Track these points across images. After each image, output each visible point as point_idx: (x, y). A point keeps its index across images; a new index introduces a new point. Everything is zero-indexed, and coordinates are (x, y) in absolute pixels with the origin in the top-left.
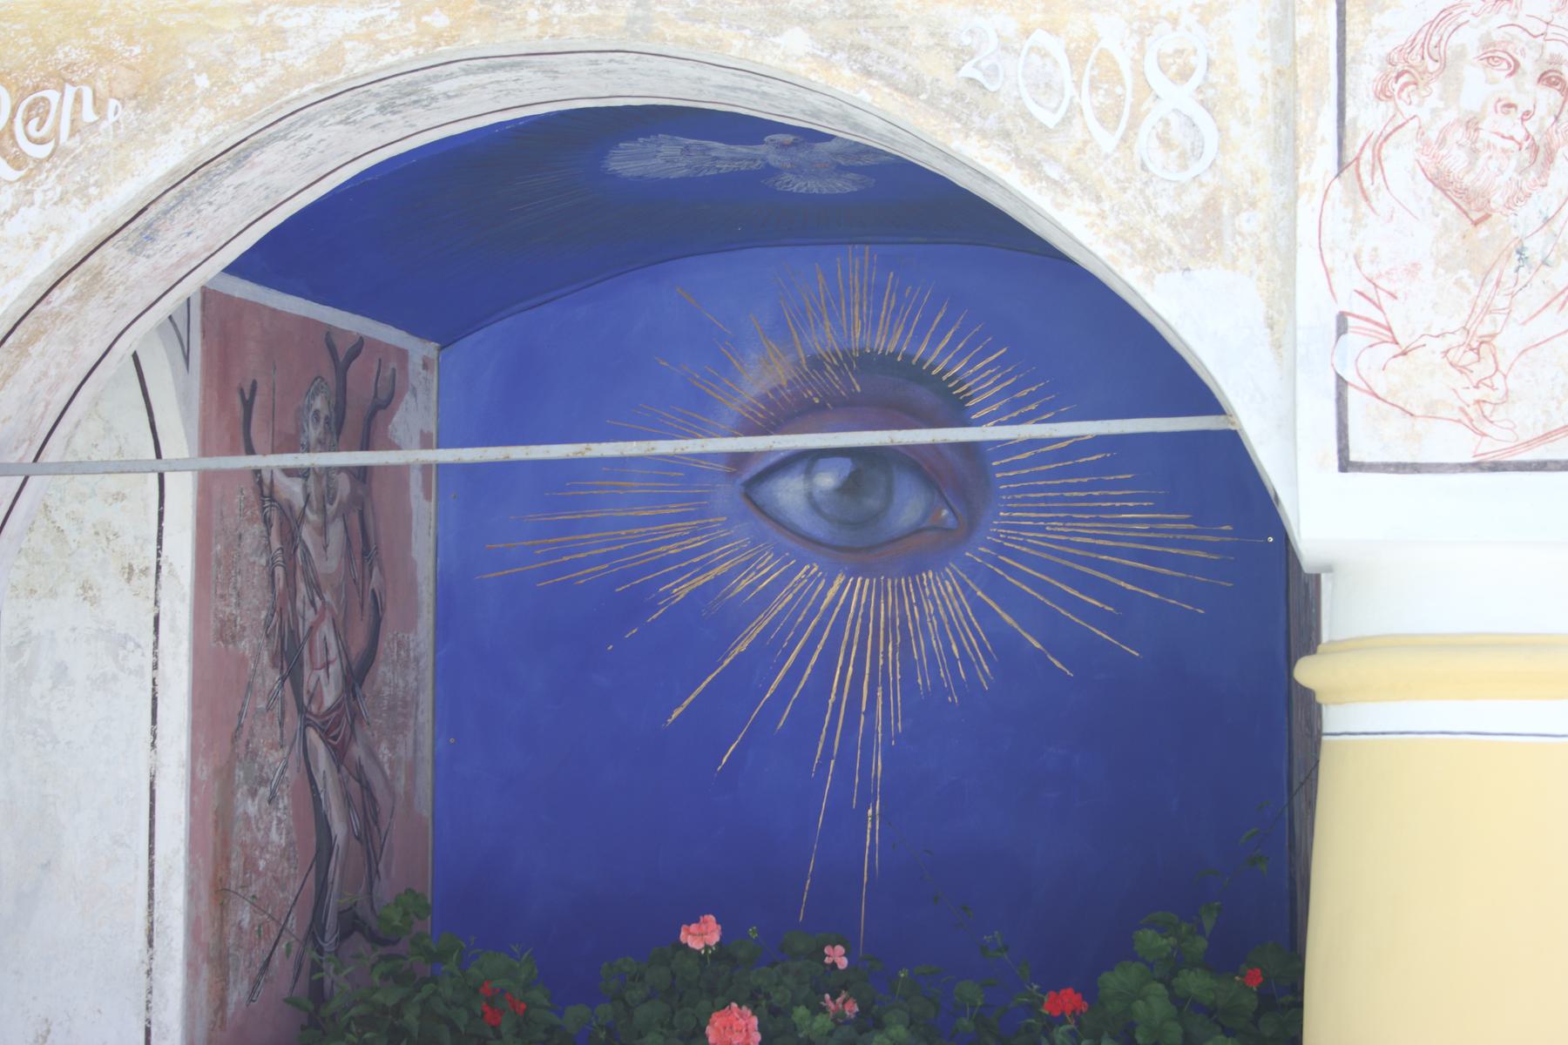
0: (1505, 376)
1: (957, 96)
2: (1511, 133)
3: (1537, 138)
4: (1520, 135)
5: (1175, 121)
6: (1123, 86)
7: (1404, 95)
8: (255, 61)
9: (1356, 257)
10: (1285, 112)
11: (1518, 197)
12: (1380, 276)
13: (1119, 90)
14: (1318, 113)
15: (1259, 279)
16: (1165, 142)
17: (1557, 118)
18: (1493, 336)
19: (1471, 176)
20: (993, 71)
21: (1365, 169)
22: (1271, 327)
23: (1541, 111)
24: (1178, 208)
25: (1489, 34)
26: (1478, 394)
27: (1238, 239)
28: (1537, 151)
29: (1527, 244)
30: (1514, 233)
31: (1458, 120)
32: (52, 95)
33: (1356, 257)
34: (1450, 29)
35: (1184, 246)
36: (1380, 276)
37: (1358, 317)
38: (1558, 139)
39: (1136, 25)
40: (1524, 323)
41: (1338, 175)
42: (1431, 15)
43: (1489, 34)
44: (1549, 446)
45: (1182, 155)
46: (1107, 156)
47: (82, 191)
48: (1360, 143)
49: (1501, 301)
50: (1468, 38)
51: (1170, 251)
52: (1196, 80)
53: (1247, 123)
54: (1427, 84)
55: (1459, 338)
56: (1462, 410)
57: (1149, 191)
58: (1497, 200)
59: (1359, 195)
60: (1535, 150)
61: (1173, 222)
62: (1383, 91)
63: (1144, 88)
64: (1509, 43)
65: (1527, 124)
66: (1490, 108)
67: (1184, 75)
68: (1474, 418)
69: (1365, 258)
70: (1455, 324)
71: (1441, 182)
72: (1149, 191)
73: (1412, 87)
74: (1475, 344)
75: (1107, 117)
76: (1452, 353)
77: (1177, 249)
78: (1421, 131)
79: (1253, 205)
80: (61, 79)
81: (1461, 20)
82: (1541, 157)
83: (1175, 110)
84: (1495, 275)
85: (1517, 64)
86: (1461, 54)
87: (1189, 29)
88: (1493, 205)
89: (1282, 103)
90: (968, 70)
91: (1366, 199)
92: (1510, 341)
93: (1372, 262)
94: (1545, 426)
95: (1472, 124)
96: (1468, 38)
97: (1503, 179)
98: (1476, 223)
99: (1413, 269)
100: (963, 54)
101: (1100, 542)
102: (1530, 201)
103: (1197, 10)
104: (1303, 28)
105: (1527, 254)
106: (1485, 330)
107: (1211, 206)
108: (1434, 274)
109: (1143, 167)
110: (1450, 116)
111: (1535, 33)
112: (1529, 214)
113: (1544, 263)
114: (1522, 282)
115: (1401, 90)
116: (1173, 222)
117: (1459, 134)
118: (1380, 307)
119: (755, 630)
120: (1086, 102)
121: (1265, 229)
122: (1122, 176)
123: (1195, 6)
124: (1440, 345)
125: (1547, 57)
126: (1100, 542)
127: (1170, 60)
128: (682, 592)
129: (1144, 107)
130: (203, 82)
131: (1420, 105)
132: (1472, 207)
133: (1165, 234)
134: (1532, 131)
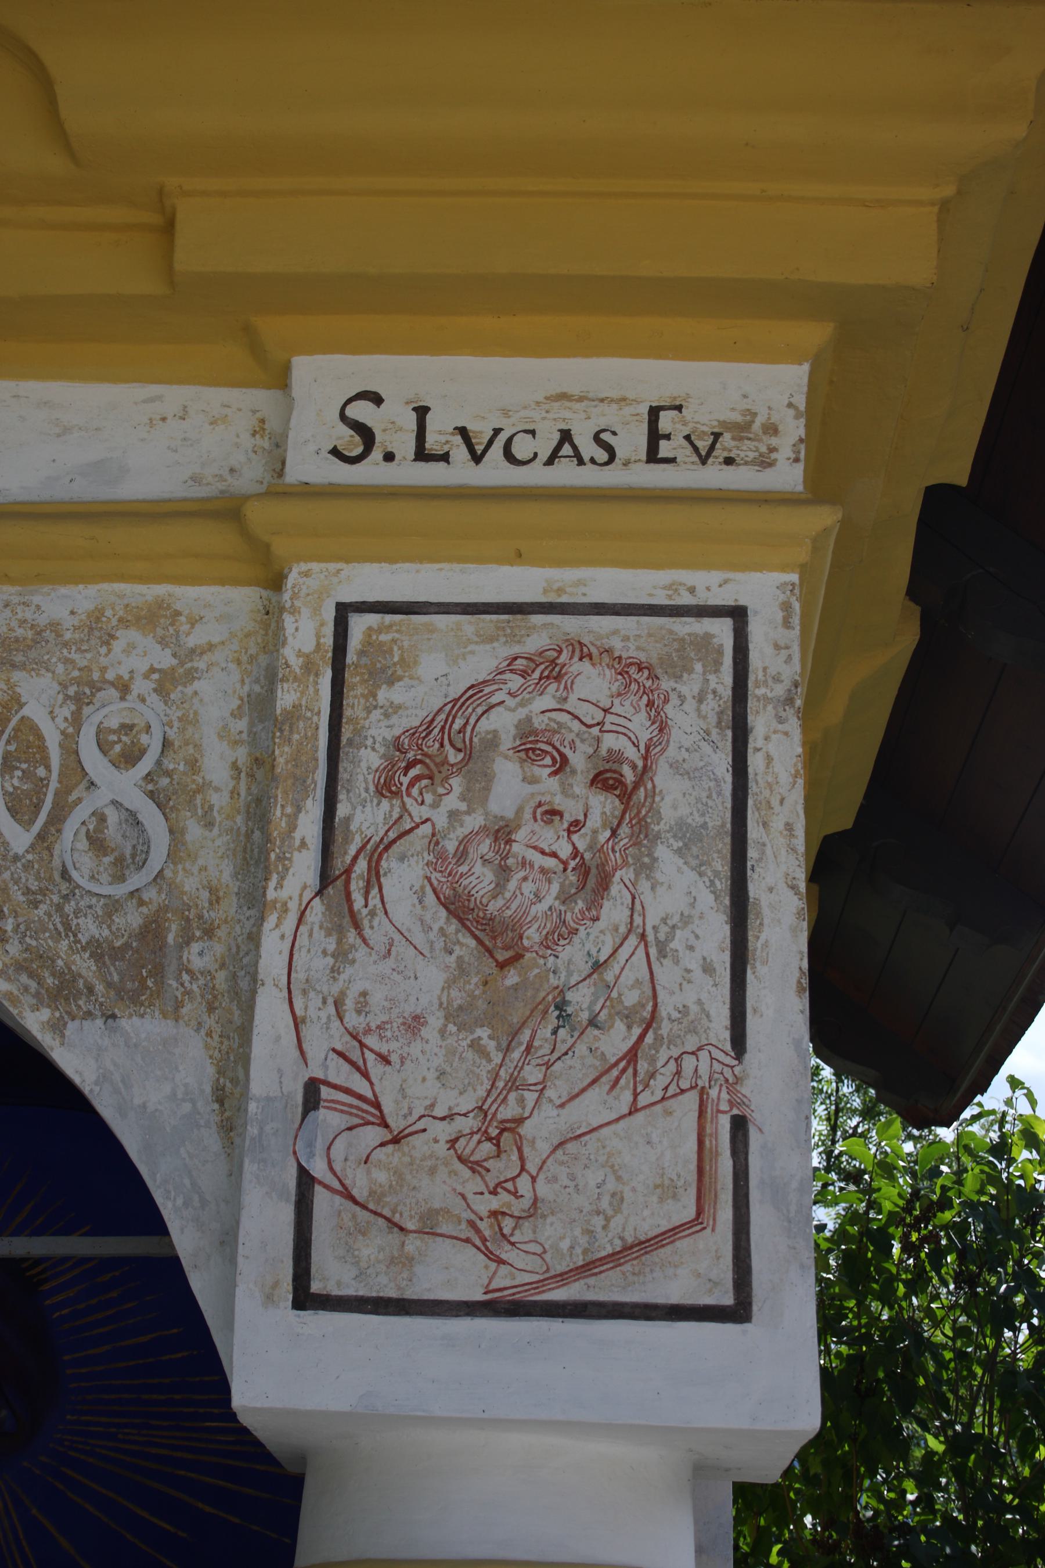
0: (534, 1179)
2: (554, 848)
3: (587, 856)
4: (565, 850)
5: (113, 817)
6: (48, 768)
7: (415, 791)
9: (338, 1004)
10: (258, 811)
11: (561, 933)
12: (368, 1031)
13: (41, 772)
14: (299, 809)
15: (209, 1034)
16: (97, 843)
17: (614, 833)
18: (520, 1121)
19: (500, 902)
21: (356, 886)
22: (221, 1101)
23: (594, 821)
24: (106, 932)
25: (529, 719)
26: (495, 1203)
27: (186, 977)
28: (587, 873)
29: (569, 996)
30: (553, 981)
31: (484, 829)
33: (338, 1004)
34: (480, 710)
35: (109, 985)
36: (368, 1031)
37: (335, 1087)
38: (615, 858)
39: (72, 691)
40: (562, 1106)
41: (319, 893)
42: (455, 692)
43: (529, 719)
44: (591, 1281)
45: (119, 861)
46: (16, 858)
48: (352, 850)
49: (532, 1074)
50: (502, 722)
51: (91, 990)
52: (146, 765)
53: (209, 825)
54: (446, 778)
55: (470, 1123)
56: (471, 1224)
57: (69, 908)
58: (532, 935)
59: (347, 919)
60: (584, 871)
61: (97, 950)
62: (387, 785)
63: (75, 771)
64: (555, 732)
65: (575, 837)
66: (527, 815)
67: (130, 758)
68: (488, 1239)
69: (349, 1004)
70: (467, 1103)
71: (458, 907)
72: (69, 908)
73: (424, 782)
74: (494, 1132)
76: (462, 1142)
77: (100, 988)
78: (434, 840)
79: (209, 933)
81: (494, 700)
82: (592, 882)
83: (114, 803)
84: (525, 1036)
85: (564, 759)
86: (492, 742)
87: (143, 700)
88: (526, 942)
89: (258, 801)
91: (357, 926)
92: (542, 1127)
93: (359, 1012)
94: (585, 1252)
95: (502, 833)
96: (502, 722)
97: (543, 906)
98: (502, 966)
99: (415, 1024)
101: (179, 1454)
102: (576, 939)
103: (156, 676)
104: (286, 698)
105: (570, 1010)
106: (507, 1112)
107: (152, 932)
108: (442, 1032)
109: (65, 874)
110: (474, 822)
111: (590, 722)
112: (573, 956)
113: (593, 1022)
114: (561, 1048)
115: (411, 784)
116: (97, 950)
117: (485, 846)
118: (365, 1075)
121: (223, 966)
122: (34, 885)
123: (153, 670)
124: (443, 1131)
125: (603, 752)
126: (179, 1454)
127: (114, 738)
129: (72, 798)
131: (435, 805)
132: (496, 940)
133: (85, 965)
134: (581, 846)
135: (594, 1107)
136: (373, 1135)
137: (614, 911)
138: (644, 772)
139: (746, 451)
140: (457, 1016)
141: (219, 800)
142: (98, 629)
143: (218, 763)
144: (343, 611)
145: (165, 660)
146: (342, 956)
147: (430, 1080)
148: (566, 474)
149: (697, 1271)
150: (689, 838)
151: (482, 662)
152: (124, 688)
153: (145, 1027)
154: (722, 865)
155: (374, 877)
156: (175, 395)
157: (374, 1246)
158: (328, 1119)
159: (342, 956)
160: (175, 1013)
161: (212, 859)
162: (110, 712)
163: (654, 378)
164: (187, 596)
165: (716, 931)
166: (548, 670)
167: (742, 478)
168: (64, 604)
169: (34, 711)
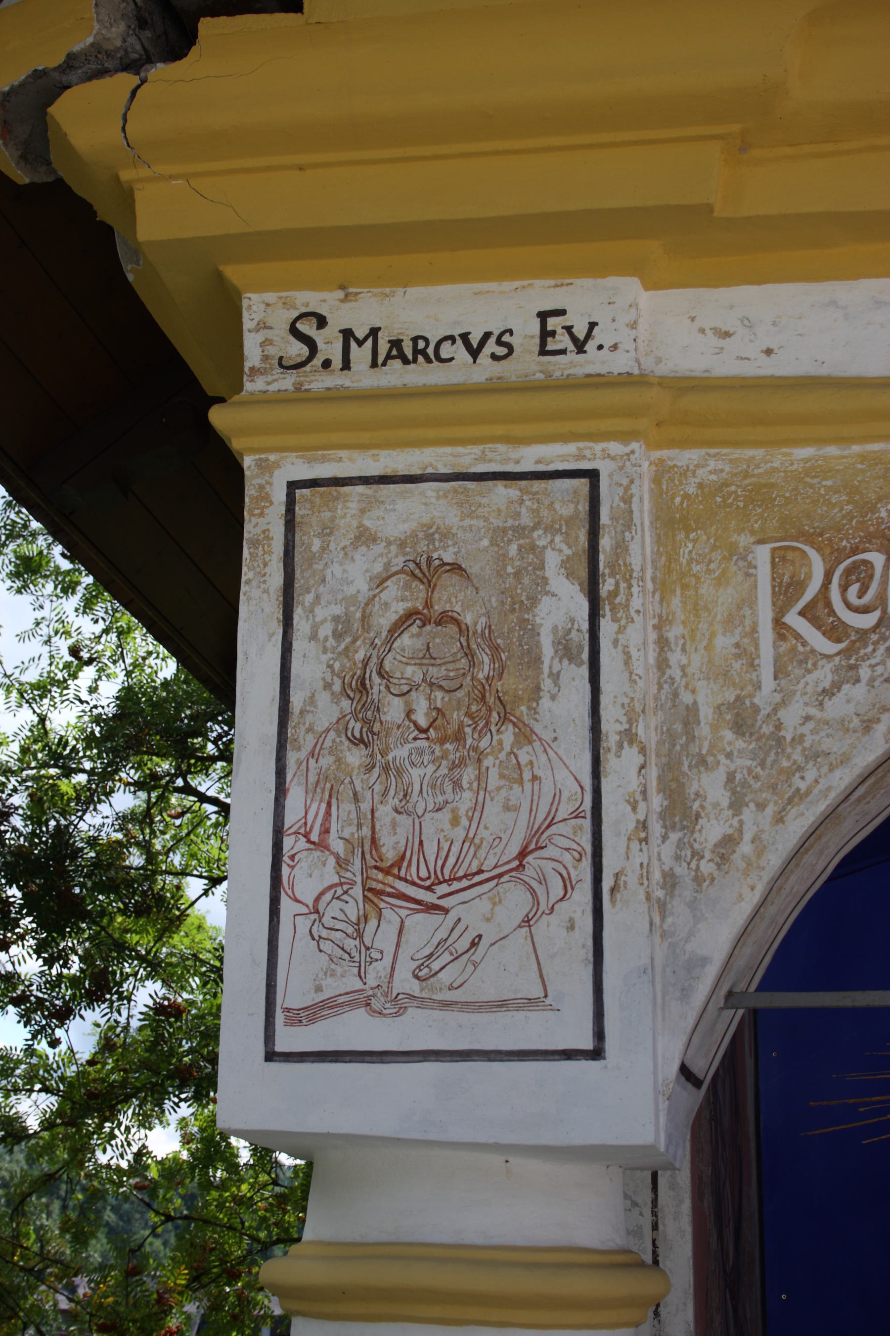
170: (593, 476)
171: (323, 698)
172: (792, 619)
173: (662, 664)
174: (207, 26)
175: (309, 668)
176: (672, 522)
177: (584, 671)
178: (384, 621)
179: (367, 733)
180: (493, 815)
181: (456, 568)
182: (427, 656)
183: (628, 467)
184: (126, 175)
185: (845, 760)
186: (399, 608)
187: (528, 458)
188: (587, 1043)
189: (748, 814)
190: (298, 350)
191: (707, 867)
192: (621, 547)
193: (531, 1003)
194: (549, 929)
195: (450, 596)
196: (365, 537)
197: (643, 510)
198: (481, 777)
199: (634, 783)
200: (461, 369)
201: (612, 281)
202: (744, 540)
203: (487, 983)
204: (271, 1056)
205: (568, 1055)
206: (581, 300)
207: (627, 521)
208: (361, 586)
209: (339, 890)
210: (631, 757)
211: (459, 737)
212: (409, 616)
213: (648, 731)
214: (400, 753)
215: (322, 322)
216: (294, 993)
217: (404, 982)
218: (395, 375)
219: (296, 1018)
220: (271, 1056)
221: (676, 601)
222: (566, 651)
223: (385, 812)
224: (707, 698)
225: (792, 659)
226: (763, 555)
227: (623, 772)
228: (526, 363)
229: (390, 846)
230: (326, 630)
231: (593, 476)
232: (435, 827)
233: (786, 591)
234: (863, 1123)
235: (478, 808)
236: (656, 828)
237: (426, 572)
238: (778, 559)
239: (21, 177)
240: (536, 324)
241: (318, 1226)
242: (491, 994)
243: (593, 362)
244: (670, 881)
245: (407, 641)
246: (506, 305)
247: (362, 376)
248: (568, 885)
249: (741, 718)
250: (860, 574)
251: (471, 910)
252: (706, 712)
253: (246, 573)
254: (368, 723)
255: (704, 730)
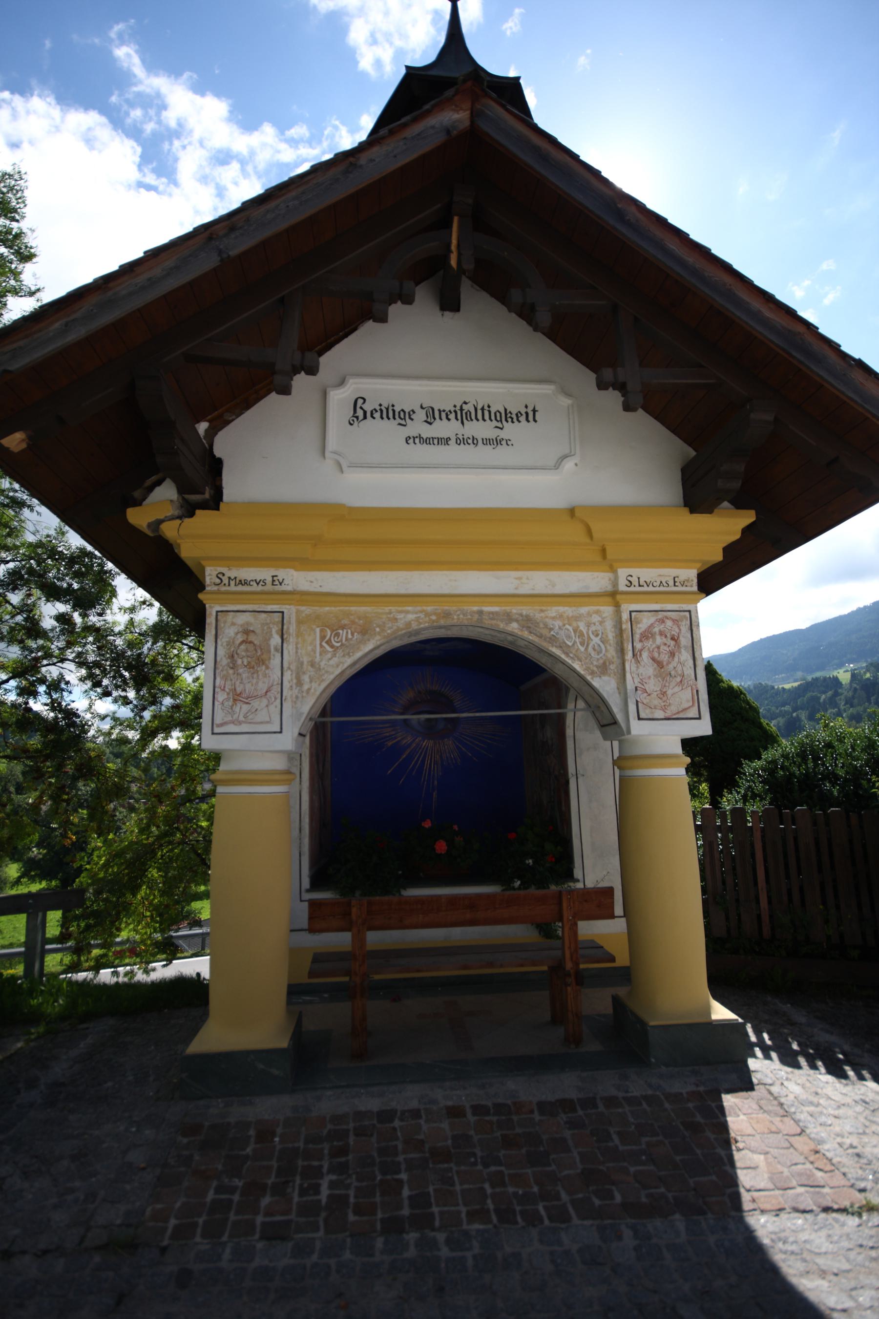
1: (550, 638)
8: (390, 625)
11: (669, 663)
16: (594, 649)
20: (557, 633)
32: (341, 631)
47: (348, 654)
50: (656, 630)
58: (665, 663)
61: (597, 667)
63: (589, 638)
71: (653, 659)
75: (582, 644)
78: (649, 649)
80: (343, 627)
90: (552, 633)
92: (670, 692)
96: (656, 630)
99: (649, 677)
100: (551, 629)
107: (604, 663)
110: (654, 646)
112: (671, 666)
116: (597, 667)
119: (407, 752)
120: (577, 640)
128: (390, 744)
130: (378, 629)
133: (595, 669)
135: (677, 689)
136: (645, 694)
137: (676, 659)
138: (678, 637)
139: (689, 584)
140: (656, 676)
141: (612, 642)
142: (589, 614)
143: (611, 636)
144: (631, 612)
145: (600, 619)
146: (638, 667)
147: (653, 686)
148: (662, 589)
149: (693, 713)
150: (686, 647)
151: (652, 620)
152: (595, 624)
153: (605, 678)
154: (691, 652)
155: (641, 655)
156: (596, 574)
157: (648, 711)
158: (639, 692)
159: (638, 667)
160: (610, 676)
161: (612, 653)
162: (593, 628)
163: (673, 572)
164: (602, 608)
165: (691, 662)
166: (662, 621)
167: (688, 589)
168: (584, 610)
169: (582, 628)
170: (283, 612)
171: (224, 659)
172: (324, 644)
173: (297, 652)
174: (198, 512)
175: (221, 652)
176: (300, 622)
177: (280, 654)
178: (238, 642)
179: (234, 666)
180: (260, 685)
181: (253, 631)
182: (247, 650)
183: (290, 611)
184: (178, 541)
185: (333, 673)
186: (241, 639)
187: (269, 608)
188: (279, 730)
189: (313, 684)
190: (218, 581)
191: (304, 694)
192: (288, 628)
193: (267, 722)
194: (272, 708)
195: (252, 638)
196: (233, 624)
197: (293, 620)
198: (258, 676)
199: (289, 678)
200: (255, 588)
201: (288, 570)
202: (314, 627)
203: (259, 718)
204: (213, 733)
205: (275, 733)
206: (281, 574)
207: (289, 622)
208: (232, 634)
209: (228, 699)
210: (289, 672)
211: (253, 668)
212: (243, 642)
213: (293, 667)
214: (241, 671)
215: (224, 575)
216: (218, 721)
217: (241, 718)
218: (240, 588)
219: (218, 726)
220: (213, 733)
221: (300, 639)
222: (276, 650)
223: (238, 683)
224: (305, 660)
225: (323, 652)
226: (318, 630)
227: (288, 676)
228: (269, 587)
229: (239, 690)
230: (225, 644)
231: (283, 612)
232: (248, 687)
233: (323, 638)
234: (478, 714)
235: (257, 683)
236: (294, 686)
237: (247, 632)
238: (321, 631)
239: (151, 534)
240: (271, 579)
241: (223, 767)
242: (259, 720)
243: (283, 588)
244: (297, 697)
245: (243, 647)
246: (264, 574)
247: (233, 588)
248: (276, 699)
249: (313, 664)
250: (337, 635)
251: (255, 704)
252: (305, 663)
253: (207, 631)
254: (234, 664)
255: (305, 666)
